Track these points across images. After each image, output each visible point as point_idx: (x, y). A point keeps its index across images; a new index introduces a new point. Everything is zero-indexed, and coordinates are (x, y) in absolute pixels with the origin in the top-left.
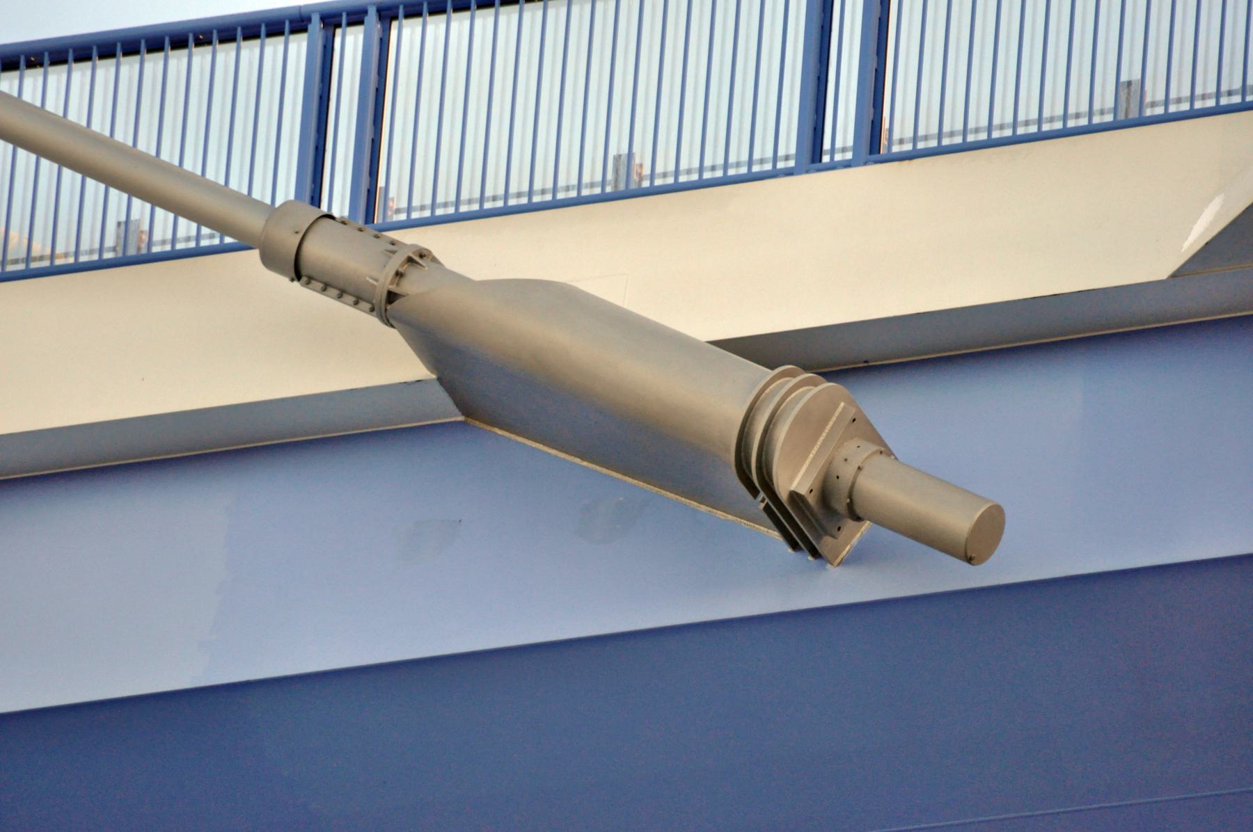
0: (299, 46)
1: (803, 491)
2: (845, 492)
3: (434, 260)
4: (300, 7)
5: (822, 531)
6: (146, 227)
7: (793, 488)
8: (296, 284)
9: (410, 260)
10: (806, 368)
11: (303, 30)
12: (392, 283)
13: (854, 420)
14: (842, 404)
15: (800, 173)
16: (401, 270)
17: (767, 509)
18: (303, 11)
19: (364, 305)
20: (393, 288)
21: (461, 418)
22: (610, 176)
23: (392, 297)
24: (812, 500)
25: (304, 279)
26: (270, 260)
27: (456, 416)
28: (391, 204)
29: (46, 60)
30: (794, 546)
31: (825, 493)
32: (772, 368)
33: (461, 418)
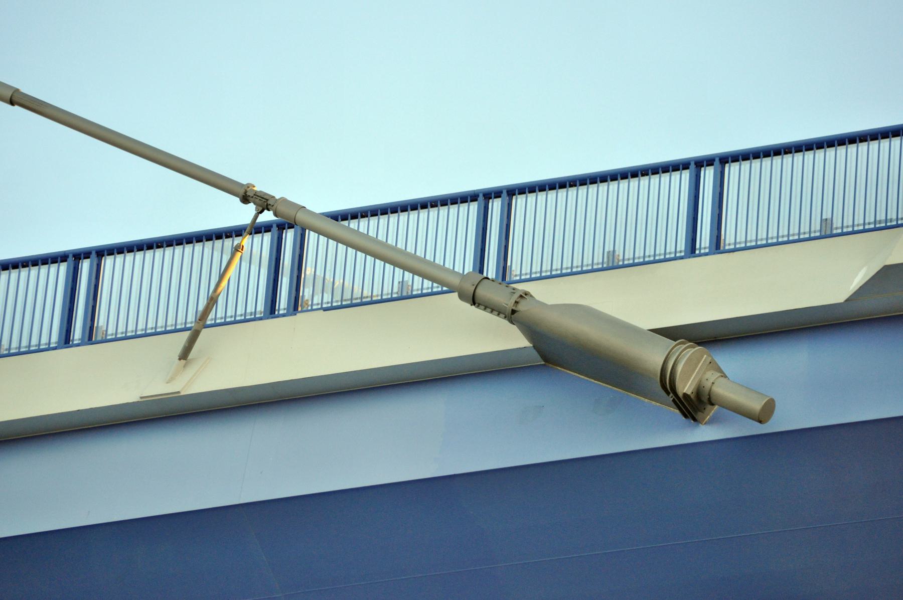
0: (63, 267)
1: (689, 393)
2: (707, 393)
3: (531, 296)
4: (474, 191)
5: (697, 410)
6: (410, 283)
7: (685, 391)
8: (473, 307)
9: (521, 296)
10: (690, 341)
11: (88, 257)
12: (514, 306)
13: (710, 363)
14: (705, 356)
15: (686, 258)
16: (517, 300)
17: (674, 400)
18: (67, 252)
19: (501, 315)
20: (514, 308)
21: (543, 363)
22: (605, 260)
23: (513, 312)
24: (692, 396)
25: (477, 305)
26: (462, 297)
27: (541, 362)
28: (513, 273)
29: (578, 183)
30: (686, 416)
31: (699, 392)
32: (675, 340)
33: (543, 363)
